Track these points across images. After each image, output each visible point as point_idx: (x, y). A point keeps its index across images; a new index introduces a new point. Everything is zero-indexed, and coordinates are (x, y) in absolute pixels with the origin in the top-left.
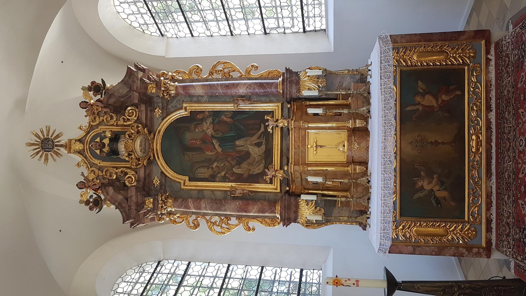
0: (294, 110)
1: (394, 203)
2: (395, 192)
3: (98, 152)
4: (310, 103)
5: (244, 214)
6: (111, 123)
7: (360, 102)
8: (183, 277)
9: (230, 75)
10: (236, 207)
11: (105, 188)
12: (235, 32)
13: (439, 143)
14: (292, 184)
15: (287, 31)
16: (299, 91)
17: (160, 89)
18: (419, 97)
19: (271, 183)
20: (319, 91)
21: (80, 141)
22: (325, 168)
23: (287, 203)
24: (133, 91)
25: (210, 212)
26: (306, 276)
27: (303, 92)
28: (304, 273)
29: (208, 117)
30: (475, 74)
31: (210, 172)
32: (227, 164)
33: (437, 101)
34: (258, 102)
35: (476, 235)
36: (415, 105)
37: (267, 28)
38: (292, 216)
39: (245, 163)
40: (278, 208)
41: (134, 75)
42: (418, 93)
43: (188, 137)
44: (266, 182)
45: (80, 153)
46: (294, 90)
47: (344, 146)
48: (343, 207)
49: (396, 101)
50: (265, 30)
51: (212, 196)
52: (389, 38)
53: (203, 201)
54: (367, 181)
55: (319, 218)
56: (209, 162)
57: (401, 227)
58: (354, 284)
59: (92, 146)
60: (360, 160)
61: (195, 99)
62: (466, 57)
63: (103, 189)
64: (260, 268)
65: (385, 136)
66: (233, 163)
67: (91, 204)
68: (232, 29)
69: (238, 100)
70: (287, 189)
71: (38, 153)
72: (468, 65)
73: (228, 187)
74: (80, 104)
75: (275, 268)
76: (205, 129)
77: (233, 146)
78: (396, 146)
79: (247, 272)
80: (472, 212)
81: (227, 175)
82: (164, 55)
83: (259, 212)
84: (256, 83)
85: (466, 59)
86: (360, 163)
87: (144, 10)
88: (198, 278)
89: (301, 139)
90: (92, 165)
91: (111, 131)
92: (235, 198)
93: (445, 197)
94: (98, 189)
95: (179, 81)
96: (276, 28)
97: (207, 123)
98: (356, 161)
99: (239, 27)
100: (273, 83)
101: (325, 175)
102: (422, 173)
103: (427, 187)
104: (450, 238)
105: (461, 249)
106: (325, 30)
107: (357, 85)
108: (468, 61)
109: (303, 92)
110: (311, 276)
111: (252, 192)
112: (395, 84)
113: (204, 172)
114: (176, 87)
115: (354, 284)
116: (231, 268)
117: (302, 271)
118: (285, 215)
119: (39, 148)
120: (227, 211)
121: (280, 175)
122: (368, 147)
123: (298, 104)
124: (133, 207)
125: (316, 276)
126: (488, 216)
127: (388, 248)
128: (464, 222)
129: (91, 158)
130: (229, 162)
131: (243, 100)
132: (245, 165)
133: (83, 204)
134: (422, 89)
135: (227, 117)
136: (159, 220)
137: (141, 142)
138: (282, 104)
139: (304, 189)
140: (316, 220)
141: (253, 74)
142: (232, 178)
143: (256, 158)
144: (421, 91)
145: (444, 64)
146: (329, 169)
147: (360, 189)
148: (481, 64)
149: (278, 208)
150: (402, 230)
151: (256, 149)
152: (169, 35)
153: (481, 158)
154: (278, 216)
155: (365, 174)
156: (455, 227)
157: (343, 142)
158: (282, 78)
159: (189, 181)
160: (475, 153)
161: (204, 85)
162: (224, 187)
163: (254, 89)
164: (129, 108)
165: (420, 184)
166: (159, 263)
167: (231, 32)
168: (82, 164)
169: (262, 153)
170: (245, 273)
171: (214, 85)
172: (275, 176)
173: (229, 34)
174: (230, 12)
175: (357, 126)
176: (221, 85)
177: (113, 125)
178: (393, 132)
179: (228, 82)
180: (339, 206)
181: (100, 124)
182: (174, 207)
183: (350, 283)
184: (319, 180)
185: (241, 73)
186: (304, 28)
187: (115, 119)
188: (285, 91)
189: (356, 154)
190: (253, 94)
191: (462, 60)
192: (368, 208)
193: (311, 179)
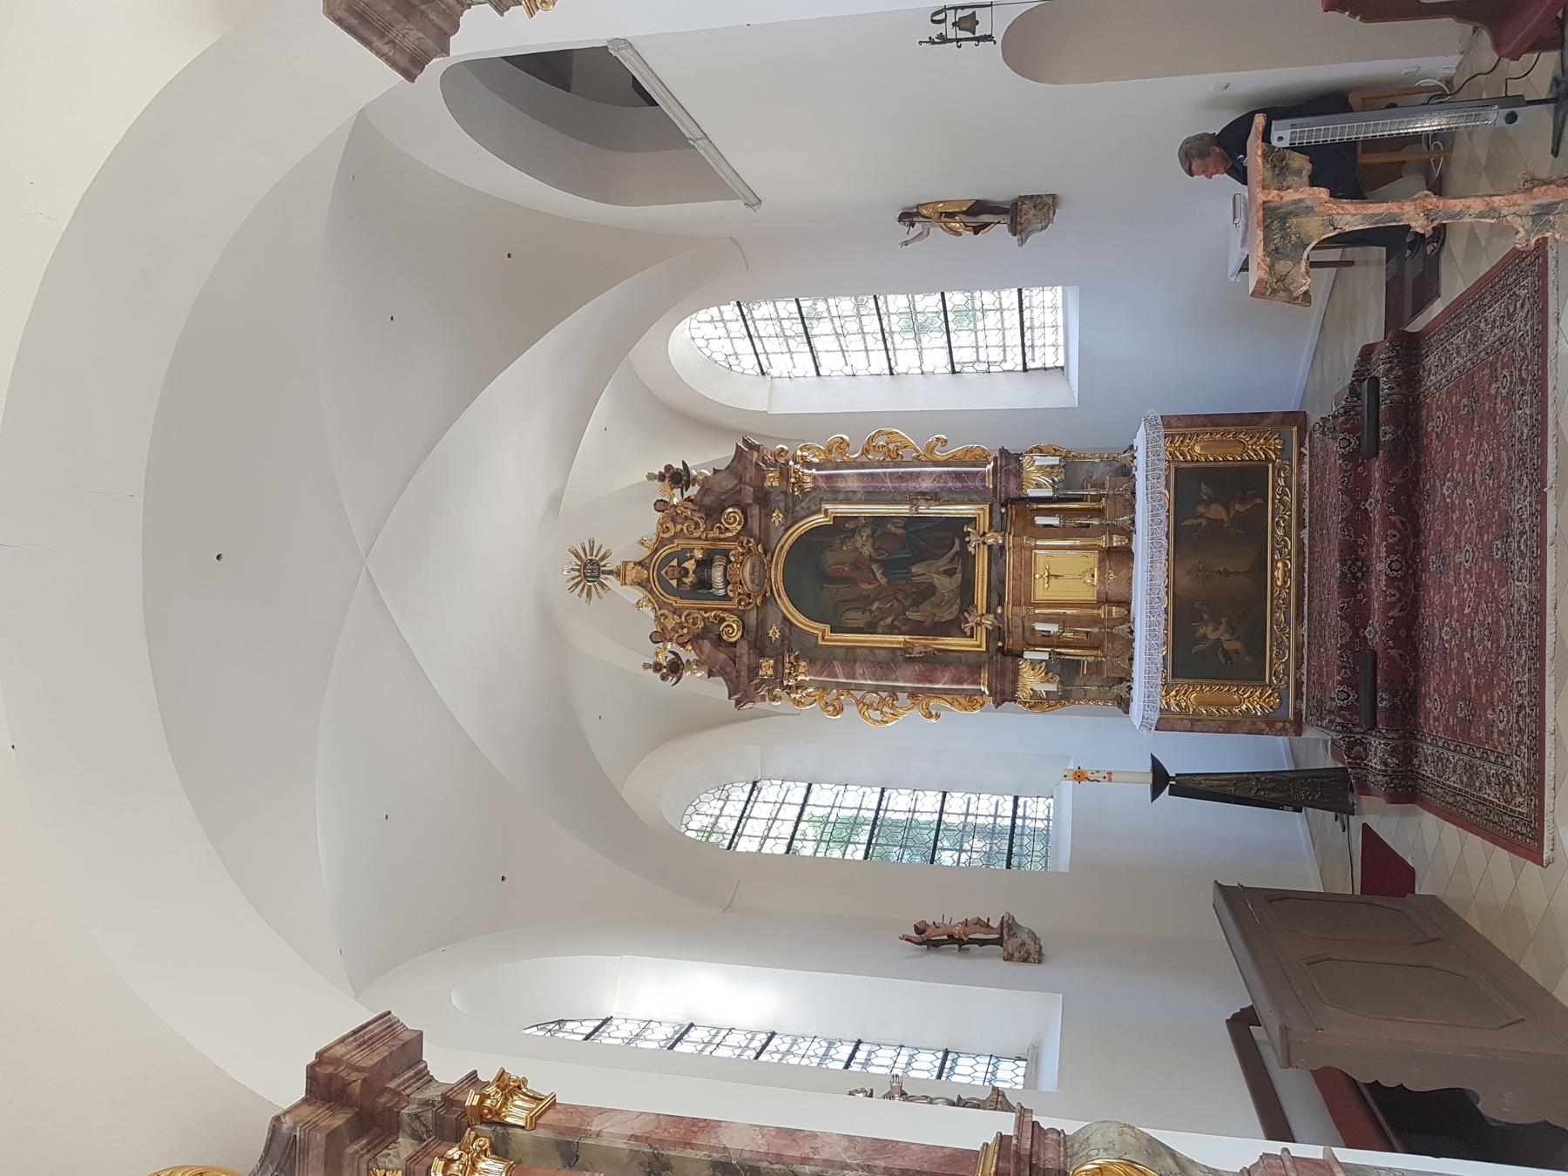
0: (1011, 519)
1: (1164, 658)
3: (674, 583)
4: (1039, 506)
5: (928, 685)
6: (696, 535)
7: (1119, 507)
9: (898, 454)
10: (915, 673)
11: (697, 642)
12: (896, 370)
13: (1230, 573)
14: (1008, 637)
15: (992, 369)
16: (1020, 487)
17: (788, 481)
18: (1203, 507)
19: (972, 636)
20: (1055, 491)
21: (640, 563)
22: (1061, 611)
23: (999, 666)
24: (745, 484)
25: (870, 682)
26: (1025, 806)
27: (1028, 491)
28: (1021, 801)
29: (863, 526)
30: (1283, 475)
31: (867, 617)
32: (896, 604)
33: (1229, 513)
34: (948, 502)
35: (1280, 703)
37: (957, 363)
38: (1008, 688)
39: (927, 602)
40: (985, 675)
41: (746, 457)
42: (1201, 501)
43: (830, 558)
44: (964, 635)
45: (644, 584)
46: (1012, 486)
47: (1093, 576)
48: (1090, 675)
49: (1168, 511)
50: (953, 367)
51: (871, 657)
54: (1129, 630)
55: (1053, 688)
56: (864, 602)
57: (1174, 693)
58: (1105, 778)
59: (666, 573)
60: (1119, 598)
61: (842, 496)
62: (1270, 449)
63: (695, 644)
64: (941, 794)
65: (1152, 562)
66: (907, 604)
67: (665, 670)
68: (893, 364)
69: (918, 500)
70: (1000, 644)
72: (1274, 462)
73: (899, 643)
74: (655, 504)
75: (968, 795)
76: (858, 545)
77: (905, 575)
78: (1168, 576)
79: (916, 800)
80: (1275, 671)
81: (896, 623)
82: (765, 409)
83: (953, 682)
85: (1270, 452)
86: (1119, 603)
87: (737, 328)
88: (829, 809)
89: (1023, 565)
90: (662, 605)
91: (702, 548)
92: (911, 660)
93: (1236, 650)
94: (687, 643)
95: (818, 466)
97: (862, 537)
98: (1113, 599)
99: (906, 361)
100: (977, 473)
101: (1062, 621)
102: (1205, 615)
103: (1212, 636)
104: (1244, 707)
105: (1259, 724)
106: (1062, 368)
107: (1114, 479)
108: (1274, 457)
109: (1028, 491)
111: (939, 650)
112: (1167, 487)
113: (857, 617)
114: (815, 478)
115: (1105, 778)
116: (886, 794)
117: (1016, 799)
118: (996, 686)
119: (580, 576)
120: (899, 681)
121: (988, 621)
122: (1131, 578)
123: (1018, 507)
124: (743, 674)
126: (1298, 676)
127: (1155, 722)
128: (1263, 687)
129: (779, 595)
130: (899, 601)
131: (927, 500)
132: (926, 607)
133: (651, 671)
134: (1206, 494)
135: (896, 527)
136: (774, 700)
137: (753, 566)
138: (991, 506)
139: (1028, 644)
140: (1046, 692)
141: (939, 455)
142: (903, 628)
143: (946, 595)
144: (1205, 497)
145: (1239, 459)
146: (1069, 612)
147: (1118, 645)
148: (1291, 460)
149: (985, 675)
150: (1175, 696)
151: (946, 580)
152: (774, 372)
153: (1289, 594)
154: (985, 689)
155: (1127, 619)
156: (1251, 693)
157: (1092, 569)
158: (992, 464)
159: (831, 632)
160: (1281, 587)
161: (862, 474)
162: (891, 642)
163: (946, 482)
164: (730, 510)
165: (1201, 631)
166: (754, 784)
167: (891, 368)
168: (645, 603)
169: (957, 588)
170: (914, 801)
171: (878, 474)
172: (978, 624)
173: (887, 372)
174: (892, 338)
175: (1115, 544)
176: (891, 474)
177: (699, 538)
178: (1164, 557)
179: (903, 470)
180: (1085, 672)
181: (675, 536)
182: (810, 674)
184: (1053, 628)
185: (917, 451)
186: (1025, 364)
188: (998, 487)
189: (1111, 588)
190: (942, 489)
191: (1264, 454)
192: (1129, 672)
193: (1039, 627)
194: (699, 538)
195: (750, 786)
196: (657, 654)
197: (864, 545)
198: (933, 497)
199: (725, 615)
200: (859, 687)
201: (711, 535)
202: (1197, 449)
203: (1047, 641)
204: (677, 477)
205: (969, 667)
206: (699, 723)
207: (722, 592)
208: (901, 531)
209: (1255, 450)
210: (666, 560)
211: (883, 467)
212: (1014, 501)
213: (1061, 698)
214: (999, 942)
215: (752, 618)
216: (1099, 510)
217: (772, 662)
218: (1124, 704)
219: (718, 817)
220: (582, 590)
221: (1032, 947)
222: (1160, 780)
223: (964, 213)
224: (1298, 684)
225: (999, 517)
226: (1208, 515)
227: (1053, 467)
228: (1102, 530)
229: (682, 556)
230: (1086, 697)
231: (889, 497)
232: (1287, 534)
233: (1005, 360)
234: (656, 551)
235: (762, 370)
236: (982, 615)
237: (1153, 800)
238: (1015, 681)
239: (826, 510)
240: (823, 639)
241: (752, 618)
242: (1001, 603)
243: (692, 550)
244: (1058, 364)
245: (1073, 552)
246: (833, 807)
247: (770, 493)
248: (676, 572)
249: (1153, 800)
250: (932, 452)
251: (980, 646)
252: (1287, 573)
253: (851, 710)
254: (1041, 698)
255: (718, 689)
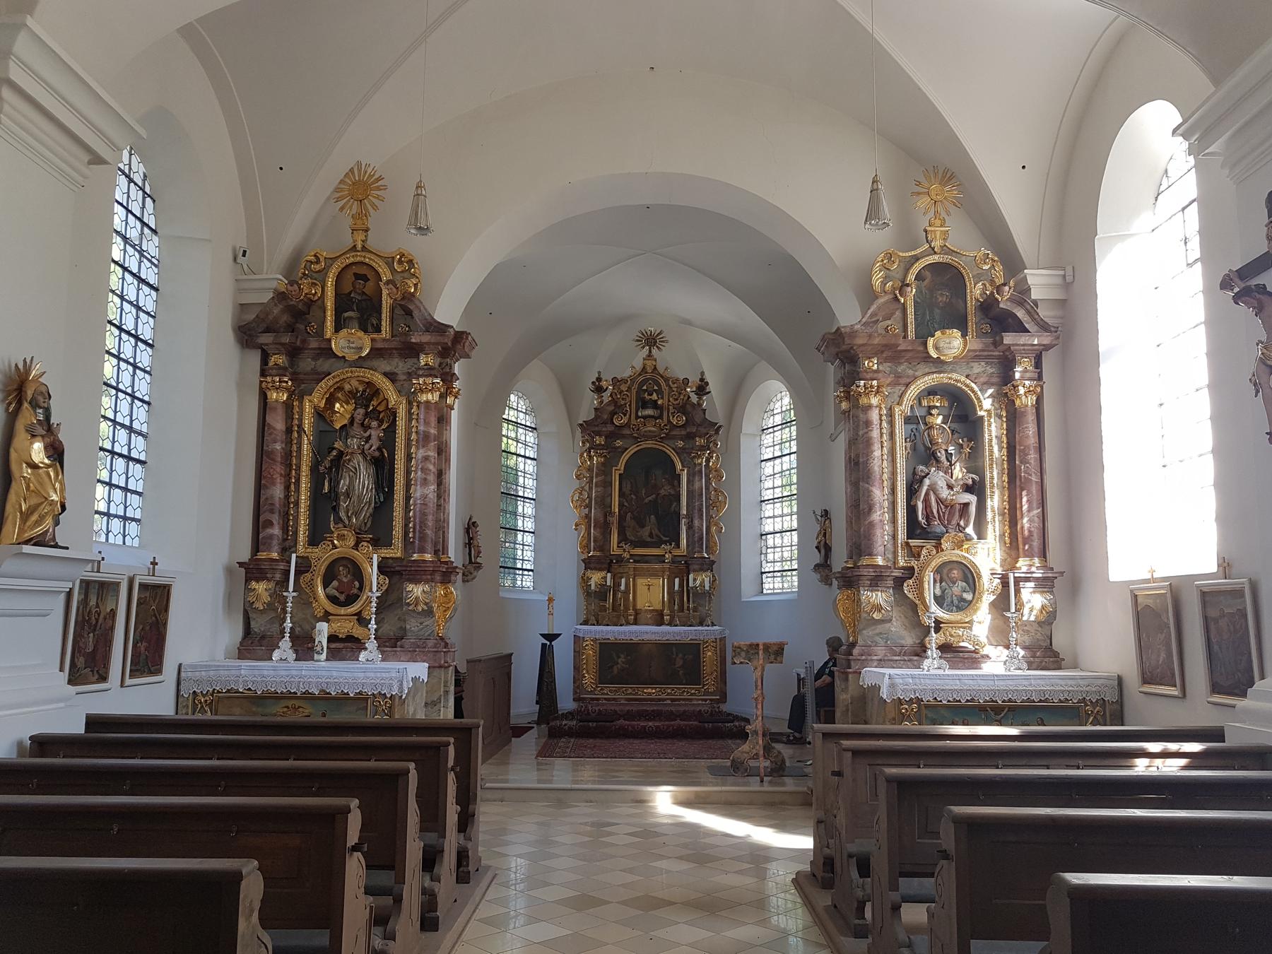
1: (609, 639)
2: (616, 639)
3: (645, 388)
5: (592, 525)
7: (684, 619)
8: (524, 457)
12: (763, 504)
16: (695, 571)
19: (618, 547)
20: (692, 588)
21: (655, 368)
25: (594, 495)
28: (531, 573)
31: (628, 492)
36: (677, 653)
38: (592, 566)
40: (598, 554)
46: (696, 567)
50: (764, 535)
52: (724, 636)
53: (602, 488)
59: (650, 384)
60: (638, 619)
68: (766, 502)
70: (614, 561)
71: (643, 334)
76: (665, 488)
83: (594, 538)
84: (702, 534)
92: (605, 516)
95: (707, 465)
96: (767, 546)
100: (703, 549)
101: (627, 592)
102: (629, 657)
103: (620, 661)
110: (528, 580)
112: (691, 640)
113: (627, 489)
114: (701, 464)
116: (532, 501)
117: (532, 571)
121: (626, 555)
125: (528, 584)
129: (638, 446)
138: (685, 556)
147: (615, 619)
148: (704, 695)
149: (598, 554)
151: (647, 534)
155: (628, 623)
160: (643, 692)
162: (614, 506)
165: (622, 656)
166: (535, 429)
167: (764, 501)
171: (702, 498)
173: (762, 499)
176: (702, 505)
177: (669, 401)
178: (657, 638)
181: (670, 388)
182: (597, 463)
183: (551, 608)
184: (623, 588)
187: (674, 402)
190: (694, 531)
193: (623, 580)
194: (669, 401)
195: (533, 426)
196: (606, 381)
197: (665, 490)
198: (690, 527)
199: (628, 416)
200: (591, 488)
201: (671, 407)
202: (710, 653)
203: (617, 585)
204: (702, 389)
205: (603, 545)
206: (569, 402)
207: (640, 414)
208: (673, 510)
209: (708, 679)
210: (659, 385)
211: (706, 499)
212: (688, 567)
213: (588, 592)
214: (471, 562)
215: (626, 432)
216: (683, 610)
217: (603, 443)
218: (586, 623)
219: (517, 410)
220: (640, 337)
221: (470, 577)
222: (551, 637)
223: (825, 542)
224: (598, 699)
225: (680, 560)
226: (678, 659)
227: (704, 587)
228: (672, 611)
229: (659, 392)
230: (589, 604)
231: (690, 504)
232: (668, 694)
233: (767, 562)
234: (662, 377)
235: (765, 429)
236: (629, 552)
237: (541, 635)
238: (595, 569)
239: (684, 470)
240: (616, 470)
241: (626, 432)
242: (635, 561)
243: (662, 398)
244: (764, 590)
245: (661, 597)
246: (524, 473)
247: (693, 439)
248: (650, 389)
249: (541, 635)
250: (715, 525)
251: (613, 551)
252: (650, 694)
253: (576, 484)
254: (587, 582)
255: (586, 414)
